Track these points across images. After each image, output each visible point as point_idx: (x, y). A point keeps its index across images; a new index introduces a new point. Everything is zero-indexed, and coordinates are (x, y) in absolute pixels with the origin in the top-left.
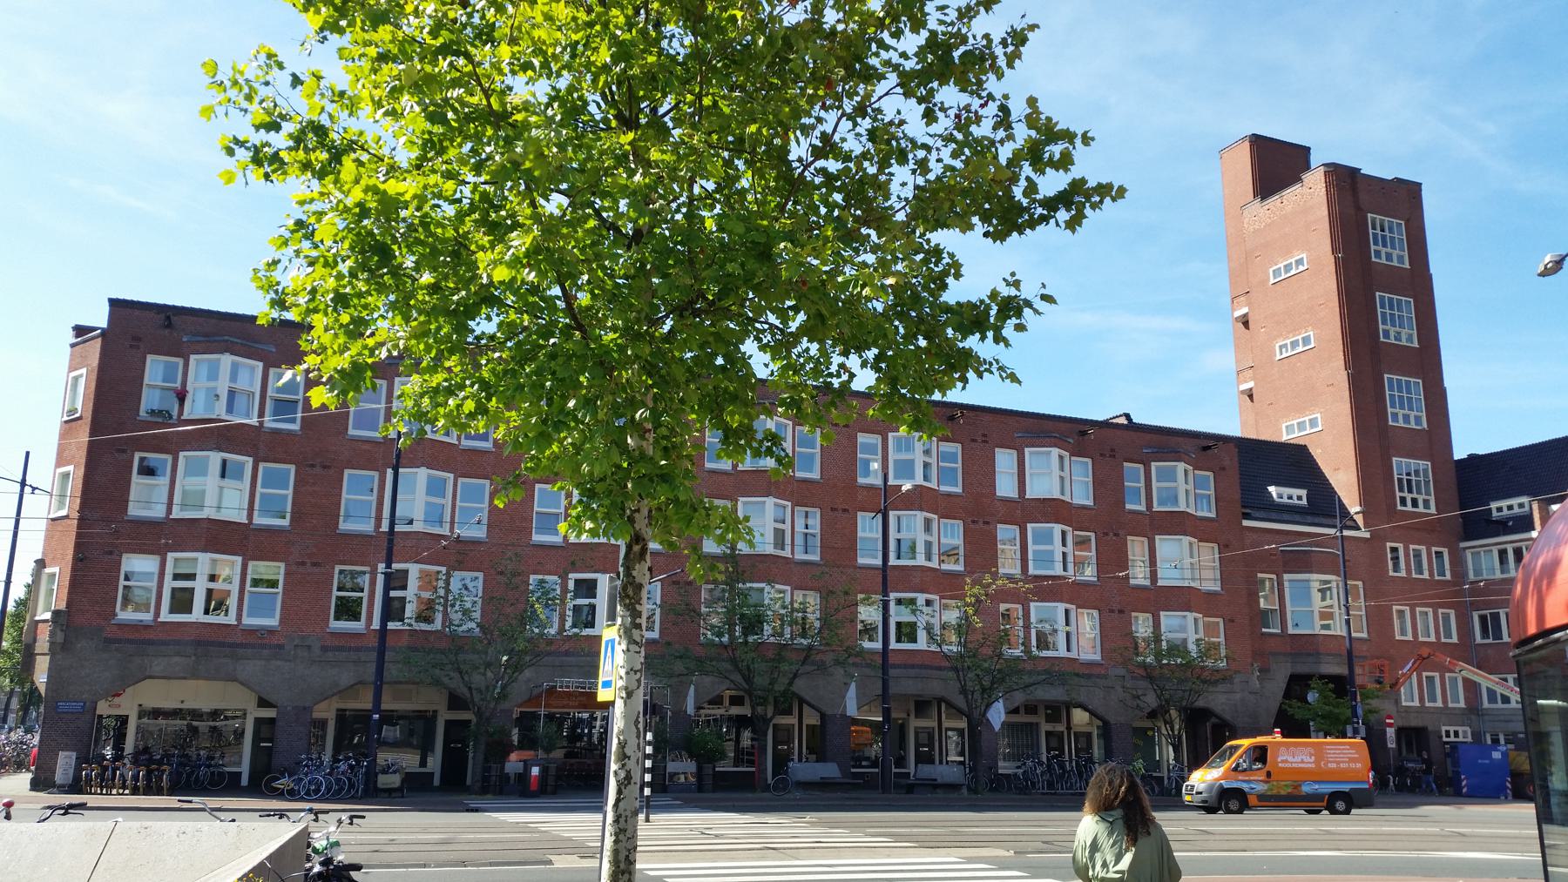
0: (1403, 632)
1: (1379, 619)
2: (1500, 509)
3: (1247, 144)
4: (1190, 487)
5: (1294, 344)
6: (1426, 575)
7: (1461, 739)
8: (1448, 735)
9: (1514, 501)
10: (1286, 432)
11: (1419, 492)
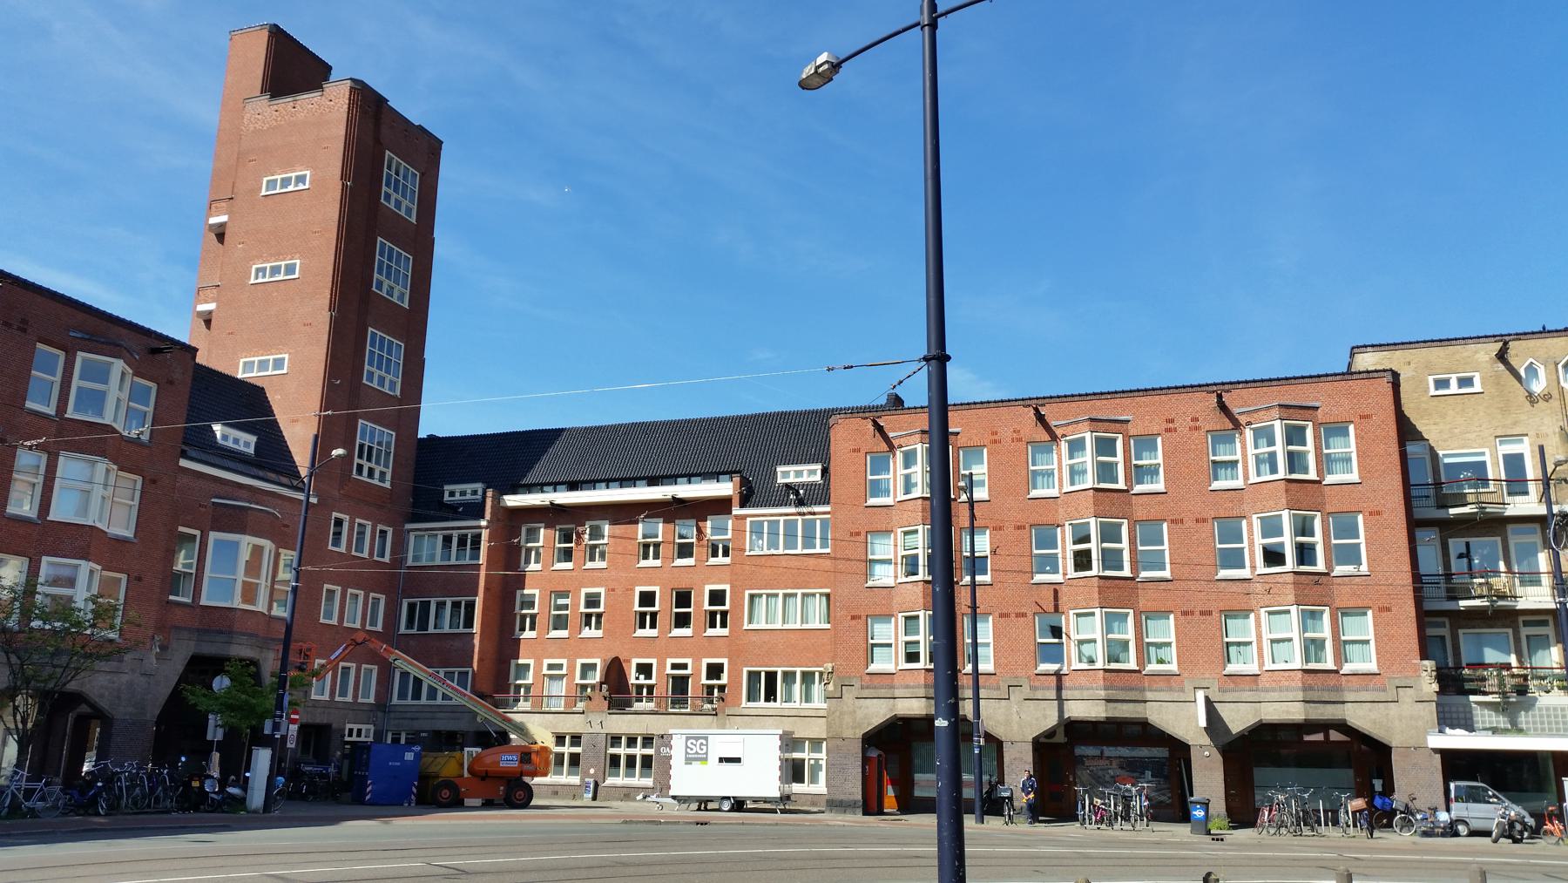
0: (329, 615)
1: (304, 595)
2: (452, 494)
3: (265, 34)
4: (125, 395)
5: (275, 271)
6: (365, 555)
7: (362, 739)
8: (351, 731)
9: (469, 487)
10: (244, 369)
11: (378, 463)
